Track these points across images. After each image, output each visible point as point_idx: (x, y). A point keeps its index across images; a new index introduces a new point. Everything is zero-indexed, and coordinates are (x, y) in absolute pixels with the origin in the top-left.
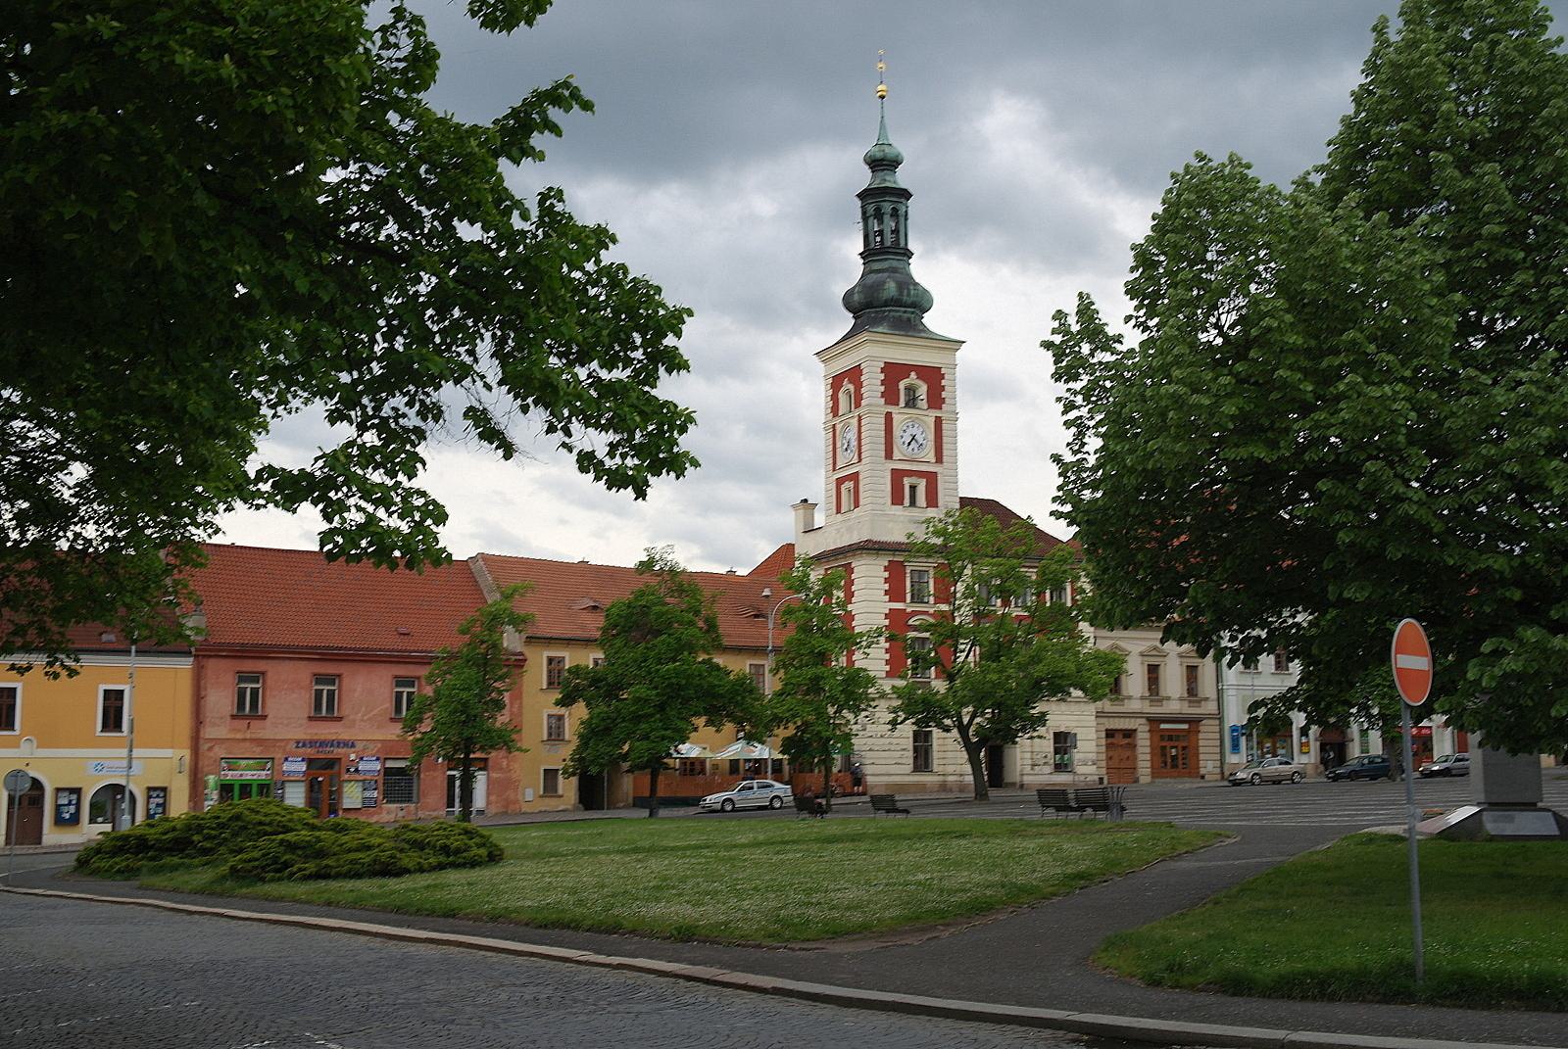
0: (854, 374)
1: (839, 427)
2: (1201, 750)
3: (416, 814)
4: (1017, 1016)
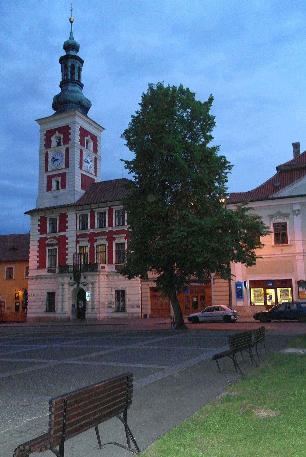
2: (213, 298)
4: (98, 430)
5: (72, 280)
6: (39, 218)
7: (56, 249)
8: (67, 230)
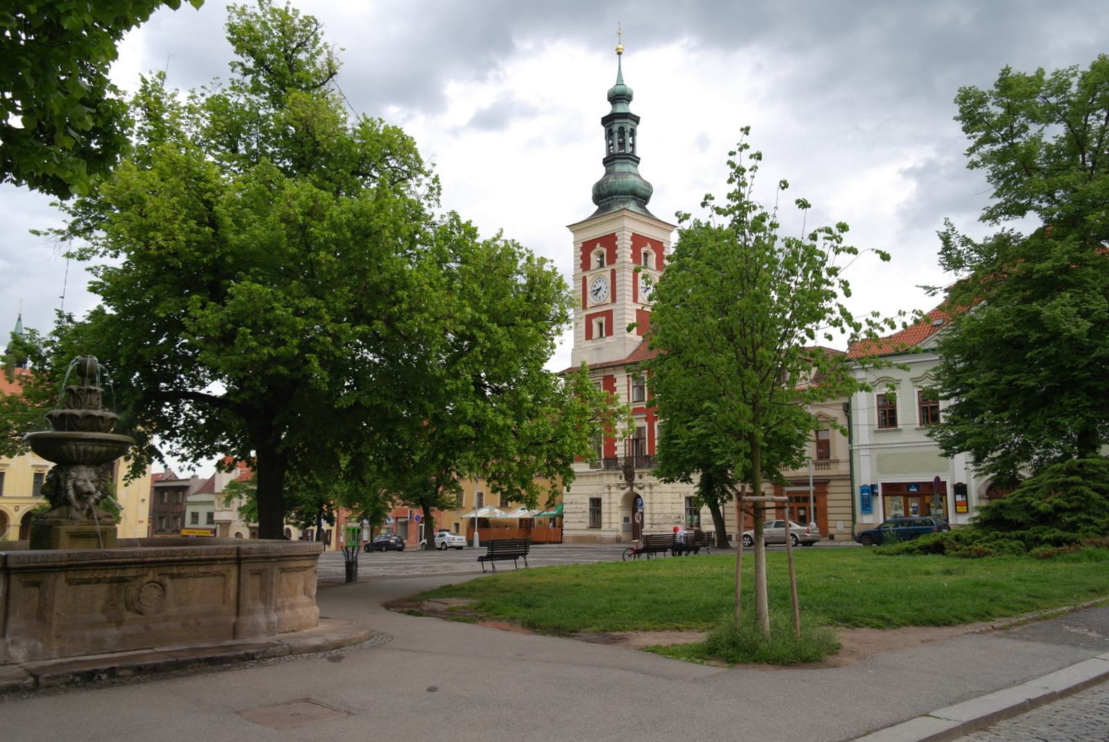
0: (609, 241)
1: (588, 279)
2: (830, 510)
8: (581, 245)
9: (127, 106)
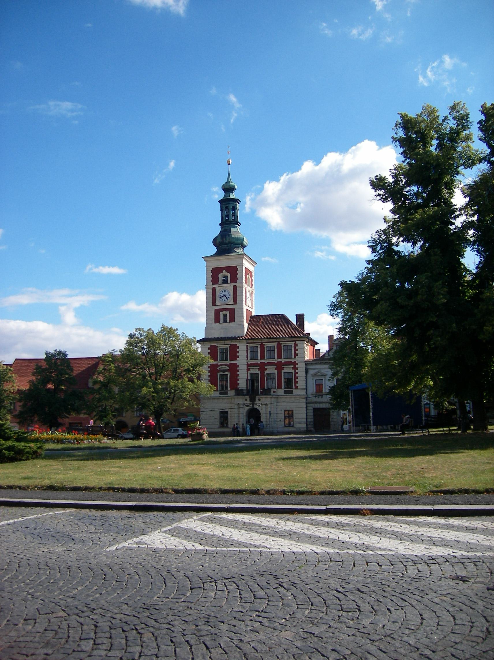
3: (310, 425)
5: (248, 402)
6: (209, 347)
7: (228, 375)
9: (454, 211)
